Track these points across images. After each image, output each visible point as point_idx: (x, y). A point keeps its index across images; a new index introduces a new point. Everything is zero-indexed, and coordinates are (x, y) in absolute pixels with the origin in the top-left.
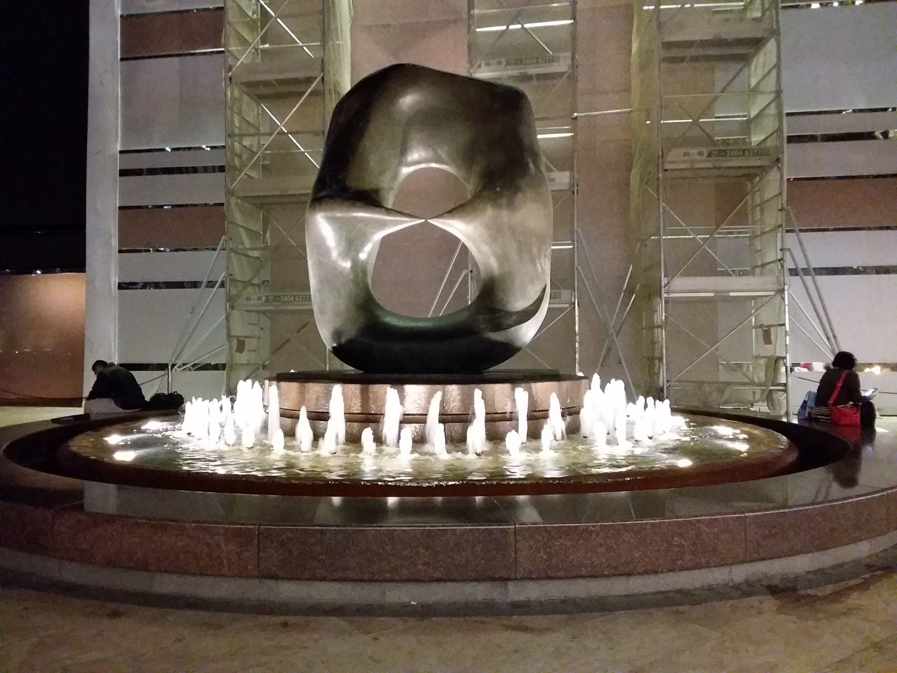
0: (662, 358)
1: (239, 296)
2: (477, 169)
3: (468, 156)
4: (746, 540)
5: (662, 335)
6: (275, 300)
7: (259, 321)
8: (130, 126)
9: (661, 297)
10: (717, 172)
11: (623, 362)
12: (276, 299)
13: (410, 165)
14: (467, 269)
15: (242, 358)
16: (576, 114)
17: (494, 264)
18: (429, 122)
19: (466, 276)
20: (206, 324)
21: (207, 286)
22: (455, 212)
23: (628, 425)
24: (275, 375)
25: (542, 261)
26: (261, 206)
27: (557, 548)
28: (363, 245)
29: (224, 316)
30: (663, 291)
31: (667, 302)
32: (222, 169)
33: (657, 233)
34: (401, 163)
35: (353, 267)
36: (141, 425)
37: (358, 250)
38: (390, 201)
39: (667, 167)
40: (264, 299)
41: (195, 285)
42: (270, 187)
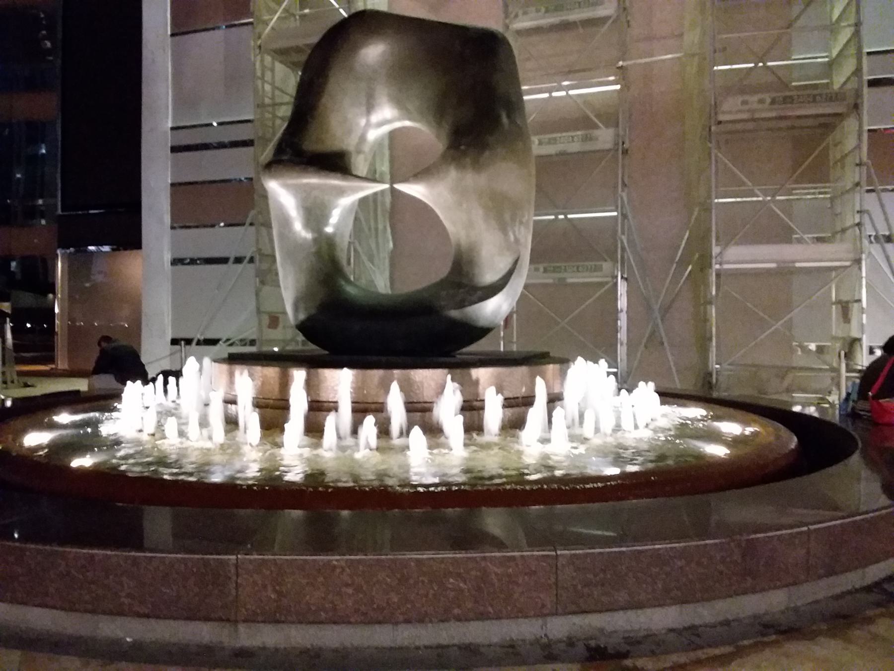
2: (447, 127)
3: (438, 111)
4: (556, 584)
8: (182, 101)
11: (666, 344)
16: (621, 63)
23: (599, 416)
24: (226, 356)
25: (516, 229)
27: (289, 585)
31: (718, 275)
35: (315, 240)
38: (360, 165)
39: (721, 118)
41: (224, 261)
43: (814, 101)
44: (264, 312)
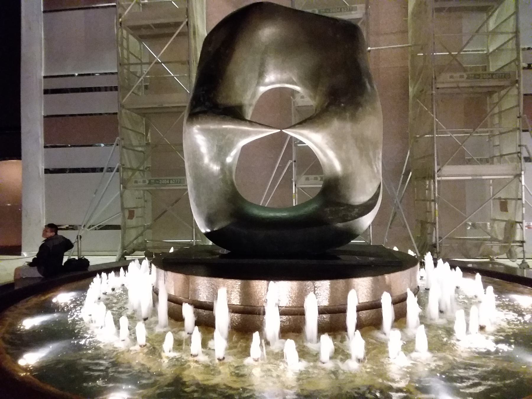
0: (435, 224)
1: (129, 180)
5: (435, 207)
6: (155, 183)
7: (144, 196)
9: (434, 178)
10: (471, 90)
12: (157, 181)
13: (266, 85)
14: (291, 159)
15: (133, 222)
16: (369, 48)
17: (338, 167)
18: (285, 49)
19: (292, 163)
20: (107, 199)
21: (108, 171)
22: (304, 124)
26: (144, 115)
28: (230, 150)
29: (119, 193)
30: (436, 176)
32: (116, 88)
33: (431, 132)
34: (258, 84)
35: (222, 170)
36: (51, 298)
37: (226, 155)
38: (249, 114)
39: (439, 86)
40: (147, 182)
42: (148, 101)
43: (492, 78)
44: (126, 208)
